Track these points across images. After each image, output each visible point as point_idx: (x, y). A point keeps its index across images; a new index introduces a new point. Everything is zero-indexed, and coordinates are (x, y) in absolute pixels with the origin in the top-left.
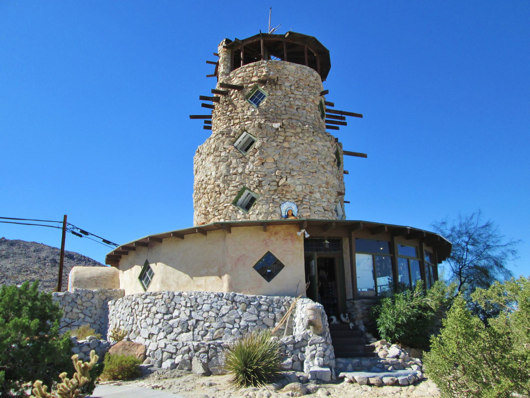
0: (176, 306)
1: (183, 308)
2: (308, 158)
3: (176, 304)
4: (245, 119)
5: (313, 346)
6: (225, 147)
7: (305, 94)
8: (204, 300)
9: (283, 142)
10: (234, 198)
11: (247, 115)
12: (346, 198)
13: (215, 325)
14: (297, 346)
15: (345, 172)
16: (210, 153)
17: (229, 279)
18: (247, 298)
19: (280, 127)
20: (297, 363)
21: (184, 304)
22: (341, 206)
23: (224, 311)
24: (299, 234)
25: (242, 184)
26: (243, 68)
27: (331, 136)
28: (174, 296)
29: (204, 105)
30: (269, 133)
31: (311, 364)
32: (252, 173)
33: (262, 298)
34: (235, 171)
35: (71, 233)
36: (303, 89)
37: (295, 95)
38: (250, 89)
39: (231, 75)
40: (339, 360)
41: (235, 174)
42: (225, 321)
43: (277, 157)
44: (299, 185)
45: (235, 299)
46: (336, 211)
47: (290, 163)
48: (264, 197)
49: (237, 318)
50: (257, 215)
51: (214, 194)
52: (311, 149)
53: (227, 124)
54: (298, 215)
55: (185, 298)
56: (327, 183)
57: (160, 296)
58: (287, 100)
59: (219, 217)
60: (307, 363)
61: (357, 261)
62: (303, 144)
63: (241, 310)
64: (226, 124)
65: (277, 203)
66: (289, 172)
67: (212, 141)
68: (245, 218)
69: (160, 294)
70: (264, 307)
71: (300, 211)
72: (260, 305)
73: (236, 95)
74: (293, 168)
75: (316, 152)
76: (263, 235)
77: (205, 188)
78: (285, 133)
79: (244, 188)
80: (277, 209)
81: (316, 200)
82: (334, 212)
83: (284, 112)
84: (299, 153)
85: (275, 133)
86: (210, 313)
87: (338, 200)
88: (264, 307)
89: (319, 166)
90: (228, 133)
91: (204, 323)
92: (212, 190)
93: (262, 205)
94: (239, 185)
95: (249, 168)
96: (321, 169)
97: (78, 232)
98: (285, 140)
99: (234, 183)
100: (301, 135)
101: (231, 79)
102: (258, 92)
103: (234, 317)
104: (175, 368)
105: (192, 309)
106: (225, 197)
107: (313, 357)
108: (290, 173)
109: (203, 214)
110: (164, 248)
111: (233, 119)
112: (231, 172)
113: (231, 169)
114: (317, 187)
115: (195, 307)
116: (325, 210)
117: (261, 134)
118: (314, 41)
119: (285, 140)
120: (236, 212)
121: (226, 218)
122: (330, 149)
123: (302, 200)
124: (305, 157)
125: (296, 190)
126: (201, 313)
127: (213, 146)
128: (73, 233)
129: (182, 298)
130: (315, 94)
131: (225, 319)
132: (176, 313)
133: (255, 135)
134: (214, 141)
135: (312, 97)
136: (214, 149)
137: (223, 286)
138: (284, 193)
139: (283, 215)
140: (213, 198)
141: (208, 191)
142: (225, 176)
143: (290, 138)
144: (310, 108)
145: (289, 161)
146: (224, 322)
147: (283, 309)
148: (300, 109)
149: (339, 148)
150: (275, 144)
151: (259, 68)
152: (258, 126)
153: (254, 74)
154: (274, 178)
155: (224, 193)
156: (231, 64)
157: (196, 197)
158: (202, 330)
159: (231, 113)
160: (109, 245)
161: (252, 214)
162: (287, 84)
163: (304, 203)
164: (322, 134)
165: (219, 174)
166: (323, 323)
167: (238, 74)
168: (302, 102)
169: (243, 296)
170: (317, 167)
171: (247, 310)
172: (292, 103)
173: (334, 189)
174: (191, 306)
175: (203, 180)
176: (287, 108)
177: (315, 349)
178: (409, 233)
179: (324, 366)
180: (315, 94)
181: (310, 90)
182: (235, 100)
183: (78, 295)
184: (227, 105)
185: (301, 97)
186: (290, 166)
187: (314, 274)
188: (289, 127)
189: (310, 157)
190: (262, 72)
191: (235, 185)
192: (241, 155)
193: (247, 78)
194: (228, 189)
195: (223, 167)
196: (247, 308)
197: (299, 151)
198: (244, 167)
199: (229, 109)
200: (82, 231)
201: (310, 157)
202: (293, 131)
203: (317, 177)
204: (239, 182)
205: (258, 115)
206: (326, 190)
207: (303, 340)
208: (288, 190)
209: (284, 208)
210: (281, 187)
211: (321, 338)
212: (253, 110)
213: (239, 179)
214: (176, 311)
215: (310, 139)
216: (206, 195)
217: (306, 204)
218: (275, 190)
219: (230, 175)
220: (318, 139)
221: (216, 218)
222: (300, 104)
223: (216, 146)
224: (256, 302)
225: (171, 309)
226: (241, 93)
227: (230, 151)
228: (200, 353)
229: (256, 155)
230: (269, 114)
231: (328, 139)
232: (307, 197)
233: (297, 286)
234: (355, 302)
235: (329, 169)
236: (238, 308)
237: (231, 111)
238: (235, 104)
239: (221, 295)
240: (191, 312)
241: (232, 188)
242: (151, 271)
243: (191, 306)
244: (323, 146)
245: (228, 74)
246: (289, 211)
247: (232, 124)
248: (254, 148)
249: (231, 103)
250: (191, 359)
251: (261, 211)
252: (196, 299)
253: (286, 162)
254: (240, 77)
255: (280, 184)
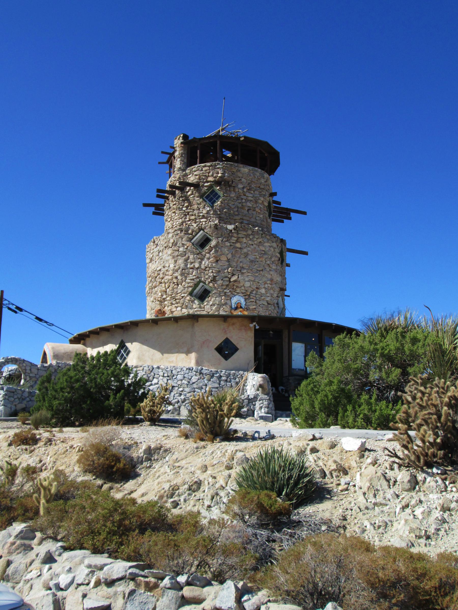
0: (154, 375)
1: (161, 378)
2: (256, 258)
3: (155, 374)
4: (200, 216)
5: (261, 401)
6: (183, 242)
7: (255, 196)
8: (178, 372)
9: (235, 243)
10: (190, 289)
11: (202, 213)
12: (286, 293)
13: (187, 390)
14: (250, 401)
15: (288, 265)
16: (168, 246)
17: (196, 358)
18: (211, 371)
19: (234, 229)
20: (250, 412)
21: (162, 375)
22: (282, 299)
23: (194, 379)
24: (252, 325)
25: (198, 277)
26: (200, 166)
27: (278, 237)
28: (153, 368)
29: (158, 196)
30: (223, 233)
31: (259, 412)
32: (207, 269)
33: (222, 372)
34: (192, 266)
35: (7, 309)
36: (254, 191)
37: (247, 196)
38: (206, 188)
39: (188, 171)
40: (277, 411)
41: (192, 268)
42: (195, 387)
43: (230, 256)
44: (248, 281)
45: (203, 371)
46: (277, 304)
47: (241, 262)
48: (218, 291)
49: (204, 385)
50: (211, 305)
51: (172, 285)
52: (259, 249)
53: (183, 219)
54: (246, 307)
55: (162, 370)
56: (272, 280)
57: (141, 368)
58: (240, 201)
59: (176, 305)
60: (257, 411)
61: (293, 348)
62: (252, 245)
63: (207, 380)
64: (182, 219)
65: (228, 296)
66: (239, 269)
67: (170, 235)
68: (200, 307)
69: (141, 367)
70: (224, 378)
71: (248, 304)
72: (221, 377)
73: (193, 192)
74: (243, 266)
75: (263, 252)
76: (223, 325)
77: (162, 278)
78: (238, 235)
79: (200, 281)
80: (228, 302)
81: (262, 295)
82: (276, 305)
83: (236, 213)
84: (249, 253)
85: (229, 234)
86: (183, 381)
87: (280, 295)
88: (224, 378)
89: (266, 265)
90: (187, 230)
91: (179, 388)
92: (170, 281)
93: (216, 298)
94: (195, 278)
95: (205, 264)
96: (267, 268)
97: (13, 307)
98: (237, 241)
99: (191, 277)
100: (251, 237)
101: (188, 175)
102: (213, 191)
103: (201, 384)
104: (168, 413)
105: (168, 378)
106: (183, 288)
107: (261, 408)
108: (240, 271)
109: (158, 301)
110: (140, 331)
111: (188, 214)
112: (188, 266)
113: (189, 264)
114: (263, 284)
115: (171, 376)
116: (268, 304)
117: (216, 234)
118: (266, 145)
119: (237, 241)
120: (193, 302)
121: (183, 307)
122: (275, 249)
123: (249, 295)
124: (254, 257)
125: (245, 285)
126: (176, 381)
127: (172, 241)
128: (10, 309)
129: (160, 370)
130: (265, 195)
131: (195, 386)
132: (155, 381)
133: (211, 235)
134: (173, 236)
135: (262, 199)
136: (173, 244)
137: (191, 362)
138: (235, 287)
139: (233, 306)
140: (170, 288)
141: (166, 281)
142: (183, 270)
143: (241, 240)
144: (260, 209)
145: (240, 260)
146: (194, 388)
147: (237, 380)
148: (251, 211)
149: (283, 247)
150: (229, 244)
151: (215, 168)
152: (214, 227)
153: (211, 174)
154: (227, 274)
155: (181, 285)
156: (187, 159)
157: (150, 285)
158: (177, 393)
159: (187, 209)
160: (41, 322)
161: (207, 305)
162: (240, 186)
163: (251, 297)
164: (269, 236)
165: (177, 267)
166: (268, 387)
167: (195, 171)
168: (252, 203)
169: (208, 370)
170: (264, 266)
171: (211, 380)
172: (244, 204)
173: (277, 285)
174: (168, 376)
175: (160, 270)
176: (239, 209)
177: (263, 403)
178: (334, 328)
179: (268, 413)
180: (265, 195)
181: (260, 192)
182: (191, 196)
183: (59, 366)
184: (183, 200)
185: (252, 199)
186: (241, 264)
187: (260, 356)
188: (241, 229)
189: (258, 257)
190: (218, 173)
191: (192, 278)
192: (198, 251)
193: (203, 177)
194: (185, 281)
195: (181, 261)
196: (211, 378)
197: (249, 251)
198: (200, 263)
199: (185, 205)
200: (17, 308)
201: (258, 257)
202: (245, 233)
203: (263, 274)
204: (195, 276)
205: (212, 214)
206: (270, 286)
207: (254, 397)
208: (238, 285)
209: (235, 300)
210: (232, 283)
211: (266, 396)
212: (208, 209)
213: (195, 273)
214: (155, 379)
215: (259, 240)
216: (163, 285)
217: (253, 299)
218: (227, 285)
219: (187, 268)
220: (265, 240)
221: (174, 306)
222: (251, 206)
223: (174, 241)
224: (218, 375)
225: (151, 378)
226: (197, 190)
227: (188, 247)
228: (186, 404)
229: (211, 253)
230: (222, 214)
231: (274, 240)
232: (254, 292)
233: (248, 364)
234: (290, 378)
235: (274, 267)
236: (204, 378)
237: (187, 207)
238: (191, 201)
239: (191, 369)
240: (168, 380)
241: (189, 281)
242: (127, 348)
243: (168, 376)
244: (270, 247)
245: (184, 170)
246: (238, 303)
247: (188, 219)
248: (210, 247)
249: (187, 199)
250: (179, 407)
251: (214, 303)
252: (172, 371)
253: (237, 261)
254: (196, 175)
255: (232, 280)
